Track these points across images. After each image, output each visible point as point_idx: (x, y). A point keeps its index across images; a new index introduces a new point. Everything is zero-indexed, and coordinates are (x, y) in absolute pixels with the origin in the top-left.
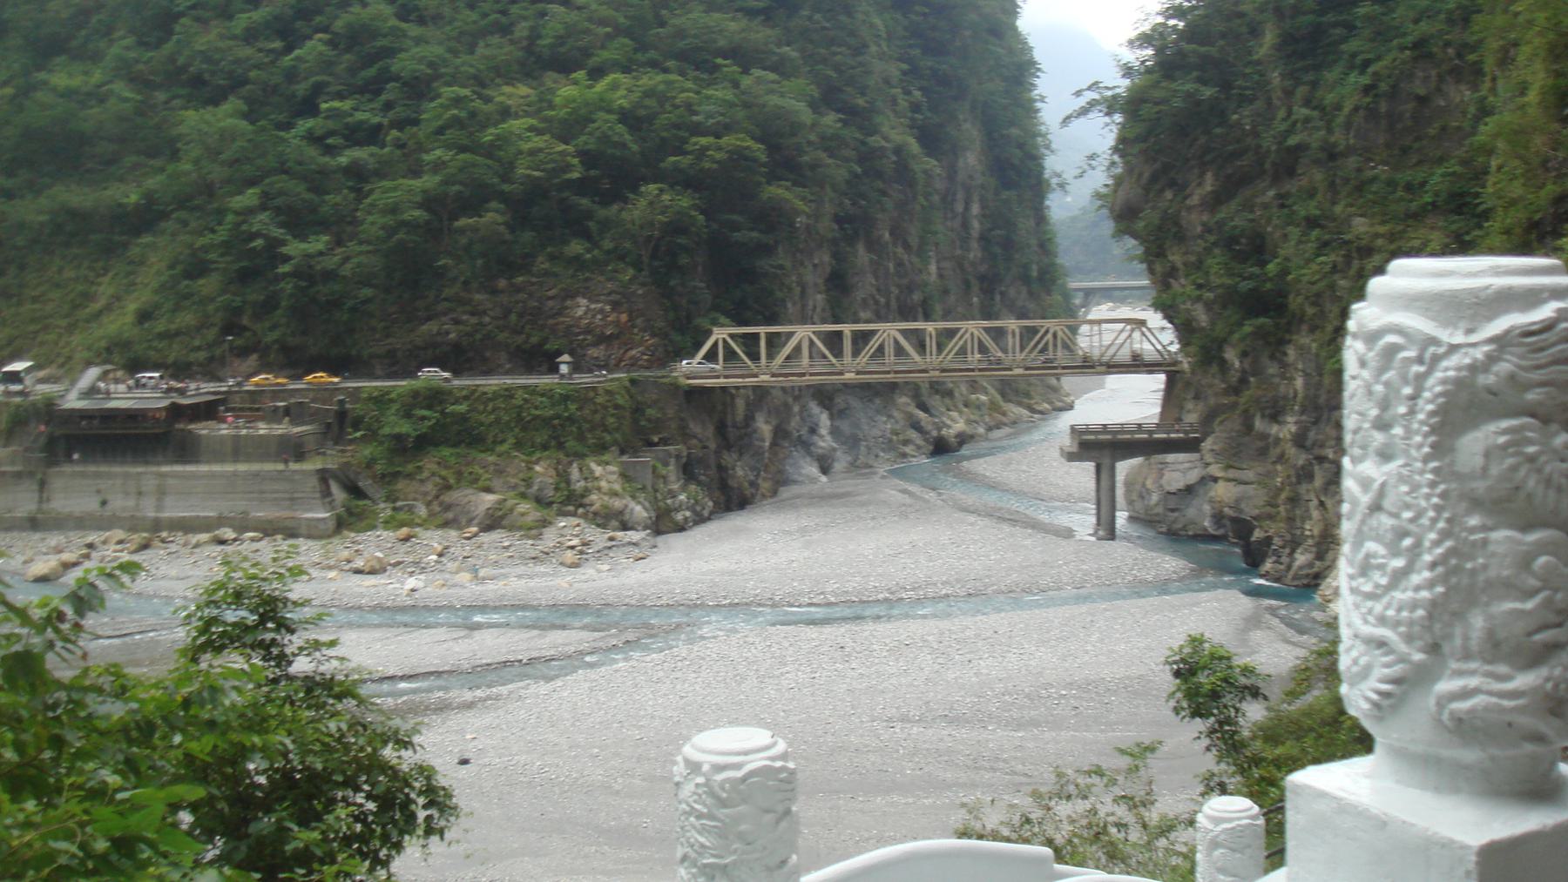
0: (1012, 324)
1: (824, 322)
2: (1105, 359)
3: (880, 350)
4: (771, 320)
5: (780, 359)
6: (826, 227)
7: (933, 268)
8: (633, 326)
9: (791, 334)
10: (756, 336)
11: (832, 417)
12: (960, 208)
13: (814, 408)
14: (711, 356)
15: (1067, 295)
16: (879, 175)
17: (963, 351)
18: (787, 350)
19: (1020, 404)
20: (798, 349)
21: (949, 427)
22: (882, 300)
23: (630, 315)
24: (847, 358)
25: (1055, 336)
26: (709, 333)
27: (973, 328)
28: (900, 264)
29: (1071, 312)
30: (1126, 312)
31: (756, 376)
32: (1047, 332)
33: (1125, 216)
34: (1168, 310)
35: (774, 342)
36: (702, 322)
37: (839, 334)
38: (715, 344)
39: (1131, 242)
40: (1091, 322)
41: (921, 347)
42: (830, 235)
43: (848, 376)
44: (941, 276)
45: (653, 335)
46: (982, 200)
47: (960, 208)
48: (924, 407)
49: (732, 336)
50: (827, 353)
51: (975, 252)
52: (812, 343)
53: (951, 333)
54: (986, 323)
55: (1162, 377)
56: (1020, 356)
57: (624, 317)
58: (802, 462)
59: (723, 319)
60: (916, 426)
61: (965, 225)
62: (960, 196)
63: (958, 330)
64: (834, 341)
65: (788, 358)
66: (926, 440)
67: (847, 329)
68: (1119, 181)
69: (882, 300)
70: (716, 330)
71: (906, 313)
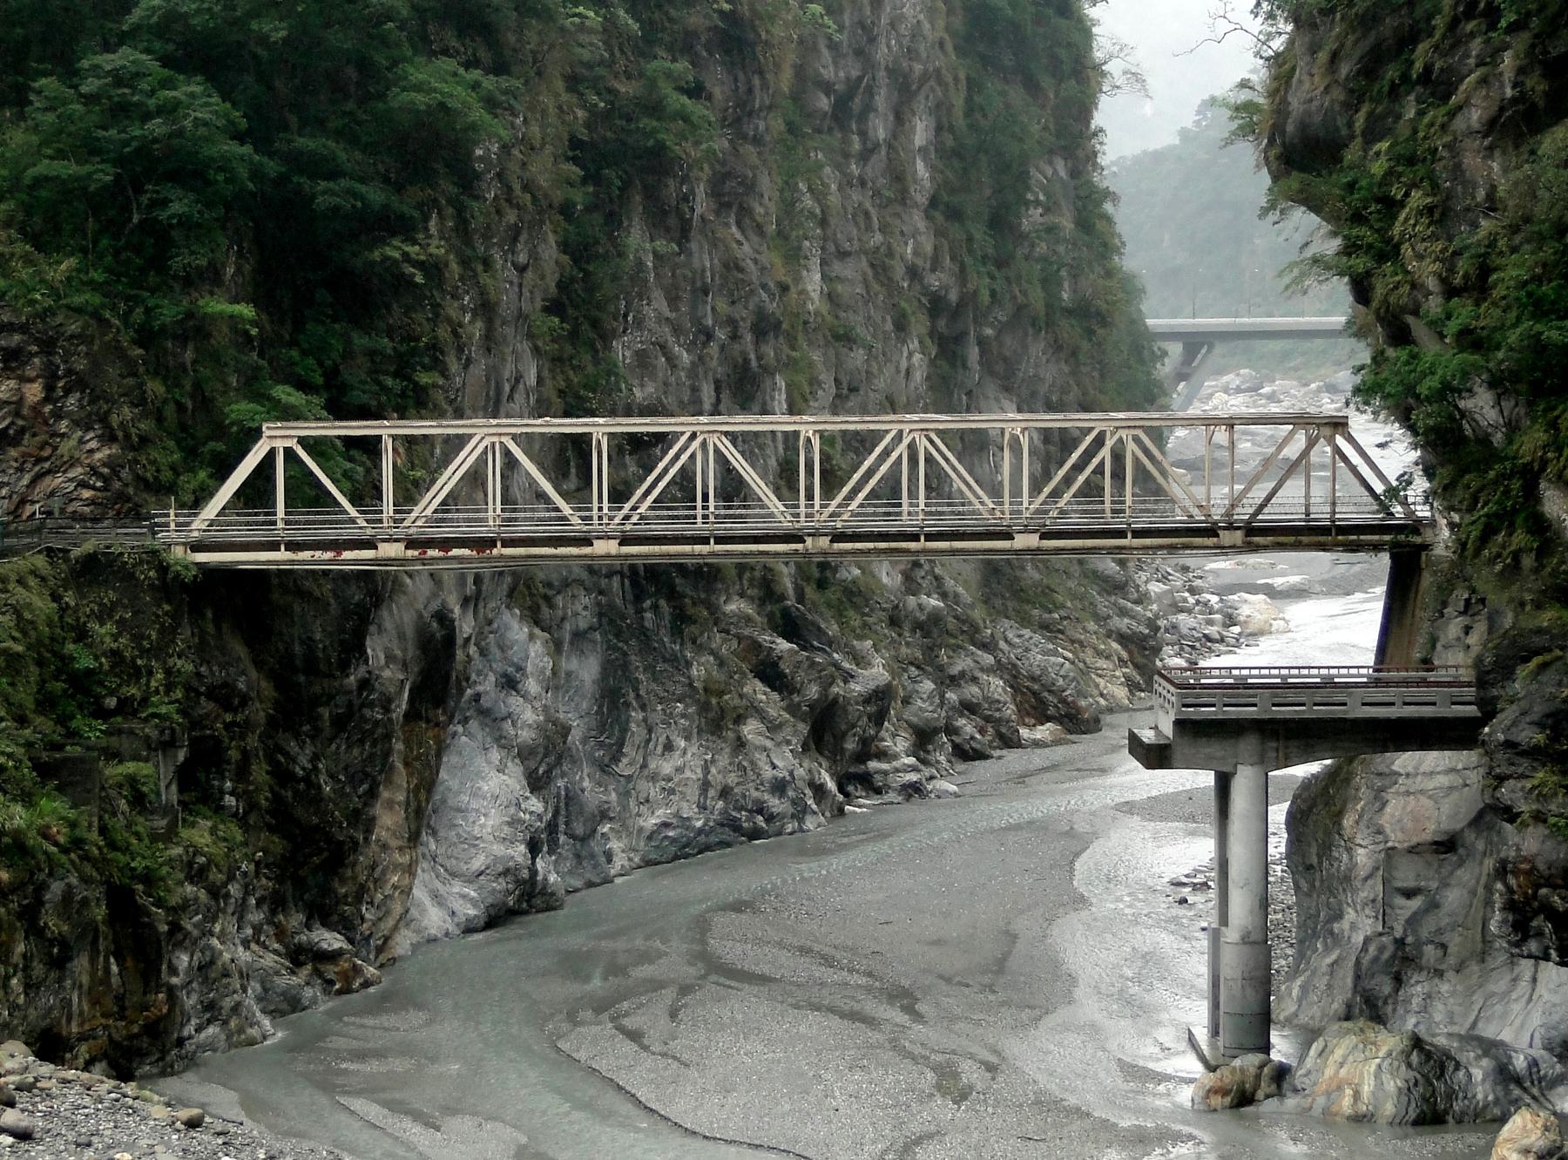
0: (1012, 423)
1: (542, 409)
2: (1243, 514)
3: (685, 483)
4: (415, 402)
5: (429, 502)
6: (548, 171)
7: (813, 282)
8: (58, 415)
9: (460, 442)
10: (370, 446)
11: (557, 647)
12: (880, 129)
13: (516, 629)
14: (256, 493)
15: (1143, 346)
16: (188, 688)
17: (889, 491)
18: (449, 478)
19: (1025, 621)
20: (475, 478)
21: (848, 677)
22: (686, 358)
23: (49, 388)
24: (600, 501)
25: (1118, 457)
26: (256, 434)
27: (912, 431)
28: (732, 266)
29: (1147, 395)
30: (1291, 395)
31: (370, 544)
32: (1099, 442)
33: (1300, 153)
34: (1393, 392)
35: (422, 461)
36: (240, 409)
37: (581, 444)
38: (272, 454)
39: (1303, 221)
40: (1190, 422)
41: (785, 480)
42: (558, 196)
43: (600, 547)
44: (831, 297)
45: (109, 437)
46: (940, 110)
47: (880, 129)
48: (790, 627)
49: (314, 446)
50: (547, 487)
51: (916, 239)
52: (510, 463)
53: (861, 443)
54: (946, 421)
55: (1385, 559)
56: (1029, 505)
57: (34, 392)
58: (480, 762)
59: (286, 394)
60: (770, 673)
61: (899, 177)
62: (881, 100)
63: (876, 437)
64: (568, 459)
65: (452, 499)
66: (793, 709)
67: (600, 429)
68: (1282, 69)
69: (686, 358)
70: (267, 429)
71: (743, 389)
